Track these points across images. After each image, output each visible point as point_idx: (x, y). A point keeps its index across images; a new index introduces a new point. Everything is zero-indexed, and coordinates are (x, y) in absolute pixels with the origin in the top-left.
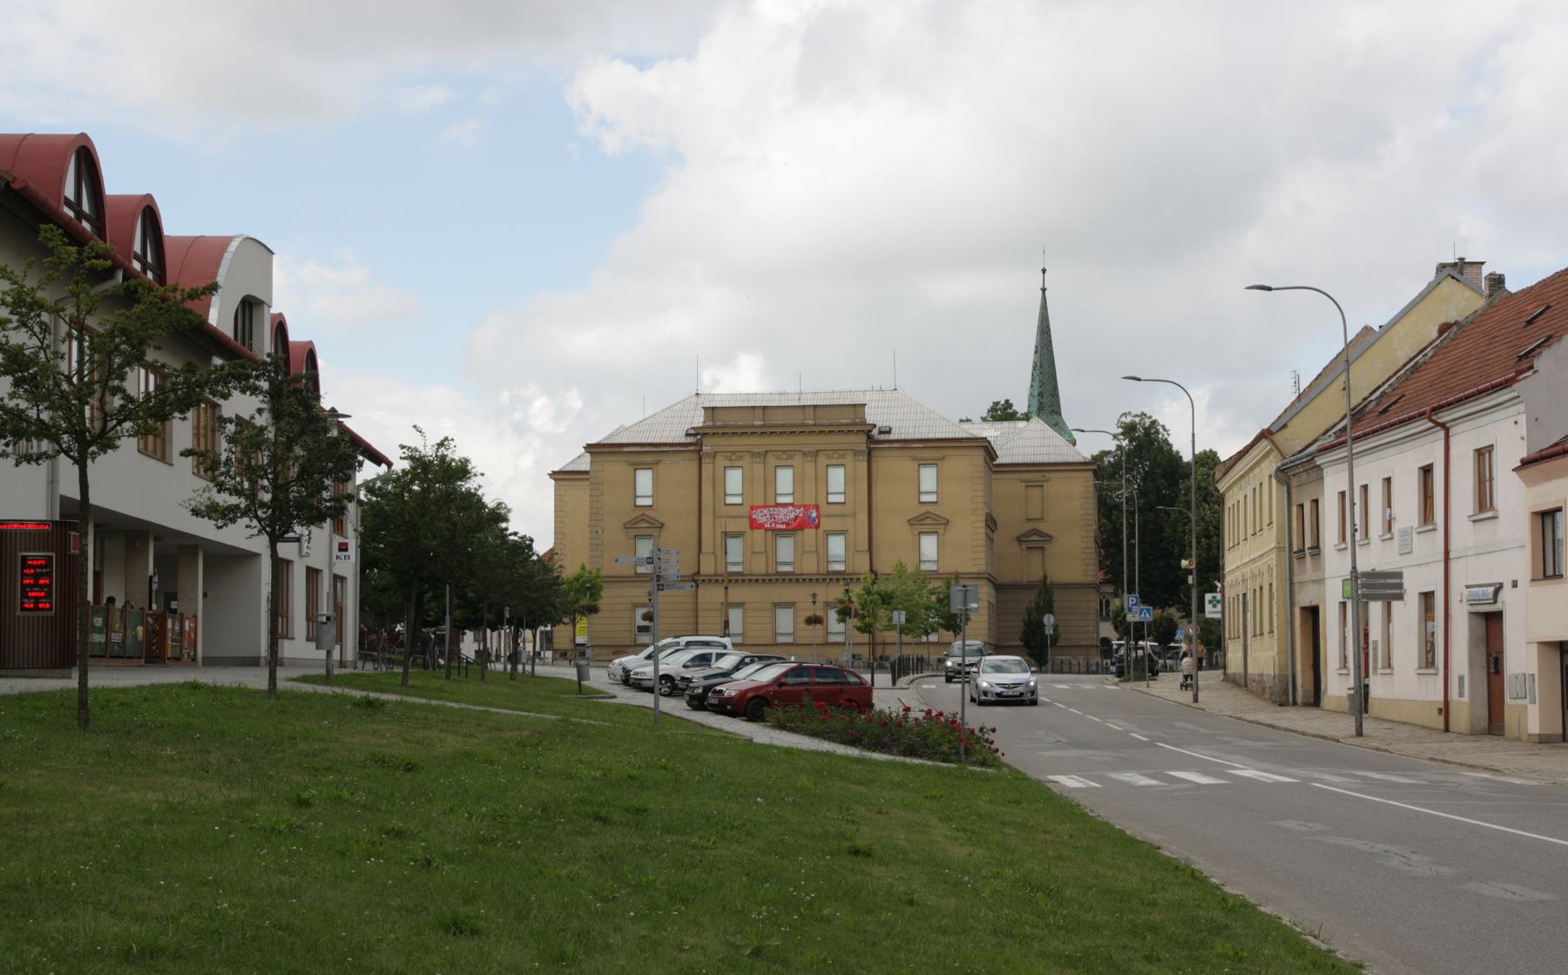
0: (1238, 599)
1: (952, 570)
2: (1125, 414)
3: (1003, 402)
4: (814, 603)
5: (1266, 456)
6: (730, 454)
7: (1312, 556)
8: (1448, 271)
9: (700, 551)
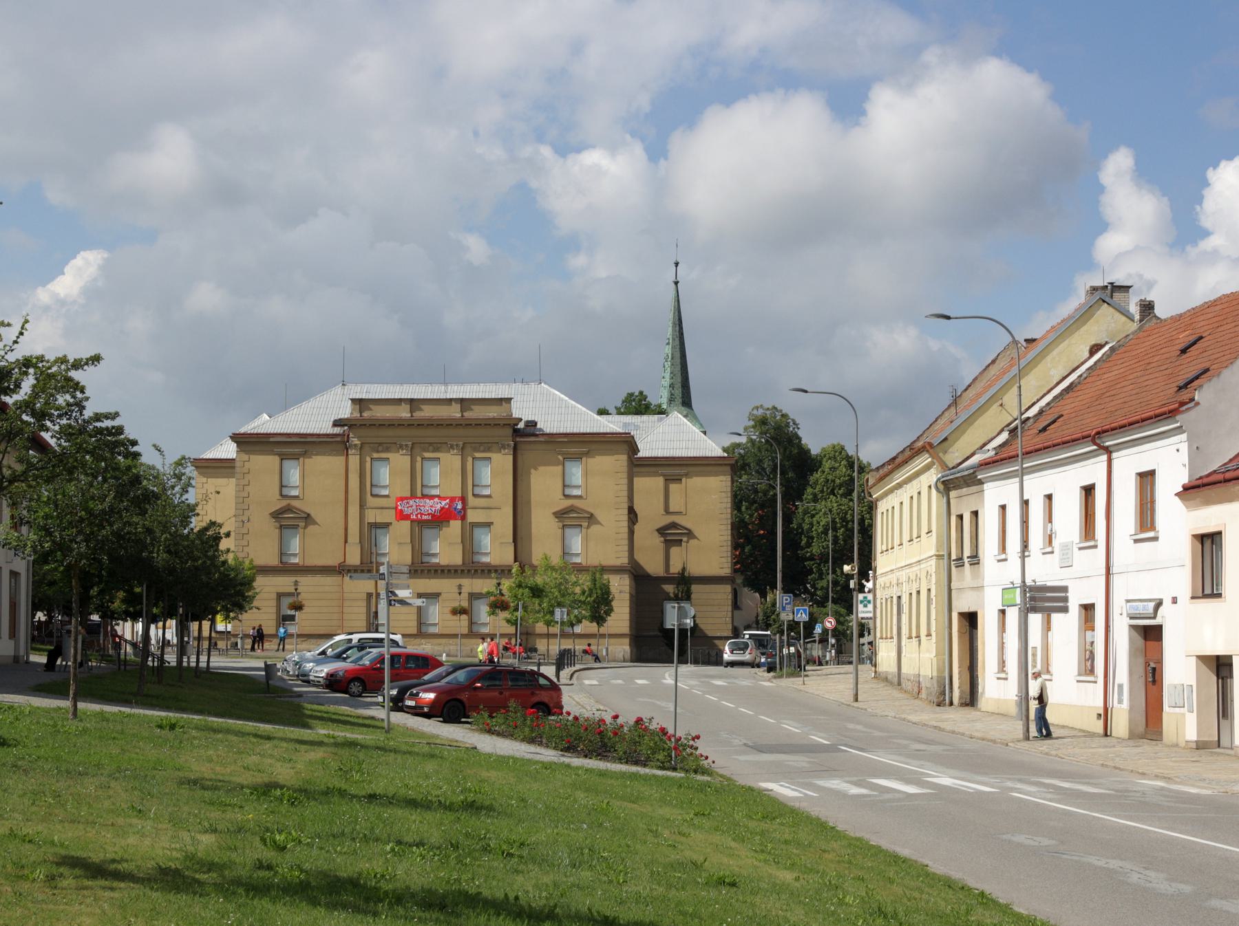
0: (892, 601)
1: (597, 564)
2: (757, 408)
3: (637, 394)
4: (460, 593)
5: (927, 468)
6: (377, 445)
7: (971, 565)
8: (1098, 295)
9: (346, 542)
